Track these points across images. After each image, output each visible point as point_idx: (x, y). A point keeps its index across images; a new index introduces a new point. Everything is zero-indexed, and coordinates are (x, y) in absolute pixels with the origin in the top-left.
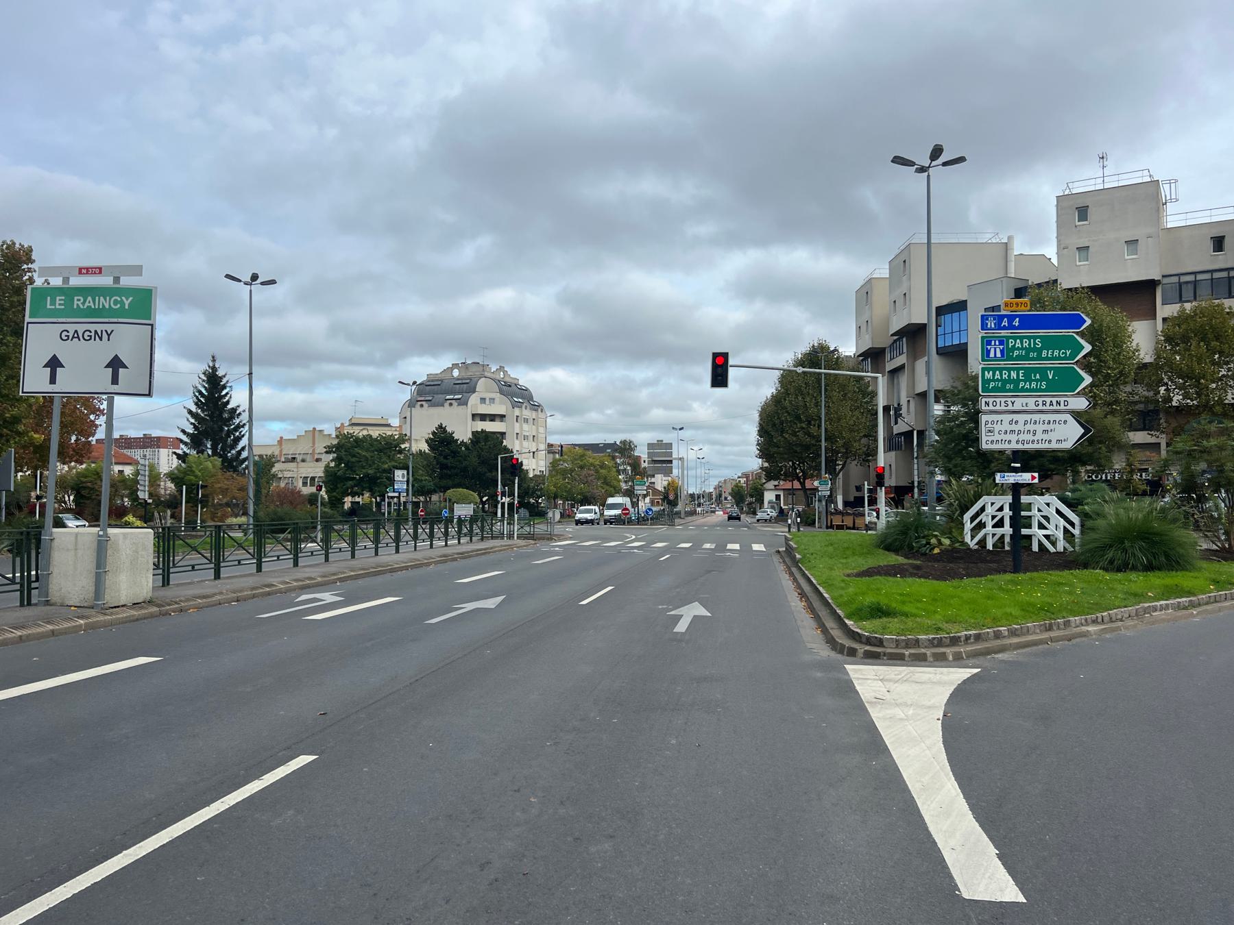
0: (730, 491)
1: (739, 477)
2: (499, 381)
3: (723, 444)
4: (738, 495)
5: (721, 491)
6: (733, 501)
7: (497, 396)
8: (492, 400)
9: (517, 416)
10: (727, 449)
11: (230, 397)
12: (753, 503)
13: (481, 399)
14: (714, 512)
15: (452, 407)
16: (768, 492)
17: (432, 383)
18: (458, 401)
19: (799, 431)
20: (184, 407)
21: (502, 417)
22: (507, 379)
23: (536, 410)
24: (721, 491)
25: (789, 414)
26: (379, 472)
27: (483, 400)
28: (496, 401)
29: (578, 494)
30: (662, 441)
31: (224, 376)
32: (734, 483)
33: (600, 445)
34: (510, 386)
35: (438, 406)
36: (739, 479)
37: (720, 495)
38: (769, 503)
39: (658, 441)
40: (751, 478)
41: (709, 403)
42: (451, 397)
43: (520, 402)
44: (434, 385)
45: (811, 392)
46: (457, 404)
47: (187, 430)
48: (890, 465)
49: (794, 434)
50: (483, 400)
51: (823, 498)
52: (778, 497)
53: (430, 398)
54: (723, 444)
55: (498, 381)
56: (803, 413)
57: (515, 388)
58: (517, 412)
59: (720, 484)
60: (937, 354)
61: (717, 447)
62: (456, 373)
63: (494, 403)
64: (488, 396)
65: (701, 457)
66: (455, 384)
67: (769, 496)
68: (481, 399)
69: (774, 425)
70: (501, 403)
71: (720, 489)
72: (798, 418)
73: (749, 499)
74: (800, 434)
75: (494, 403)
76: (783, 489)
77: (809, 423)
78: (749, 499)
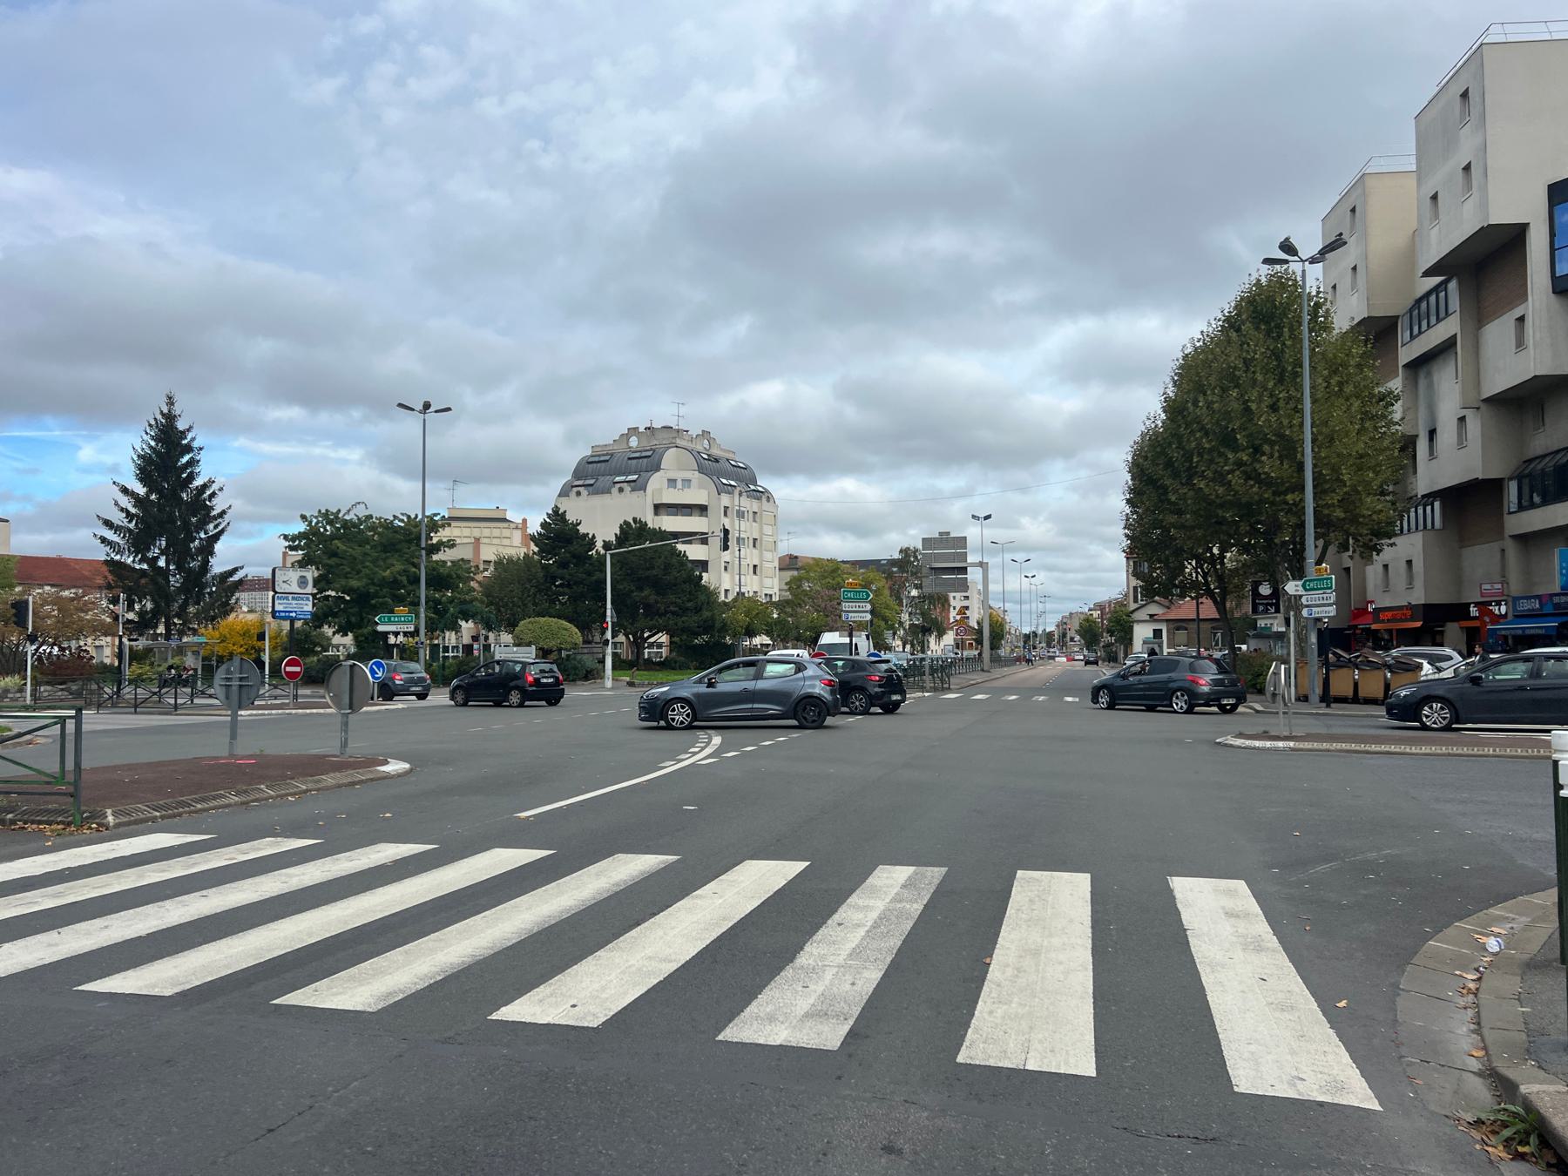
0: (1077, 626)
1: (1090, 610)
2: (699, 453)
3: (1065, 571)
4: (1089, 633)
5: (1065, 629)
6: (1083, 642)
7: (695, 476)
8: (687, 482)
9: (726, 508)
10: (1071, 576)
11: (402, 514)
12: (1112, 644)
13: (669, 480)
14: (1052, 658)
15: (623, 494)
16: (1141, 625)
17: (596, 459)
18: (632, 484)
19: (1231, 472)
20: (114, 483)
21: (702, 509)
22: (715, 452)
23: (759, 499)
24: (1065, 629)
25: (1207, 434)
26: (374, 584)
27: (672, 482)
28: (692, 483)
29: (806, 630)
30: (948, 533)
31: (188, 430)
32: (1082, 617)
33: (883, 562)
34: (717, 461)
35: (602, 493)
36: (1091, 612)
37: (1064, 635)
38: (1144, 643)
39: (941, 534)
40: (1107, 610)
41: (1041, 519)
42: (623, 478)
43: (730, 485)
44: (599, 462)
45: (1259, 377)
46: (630, 489)
47: (116, 522)
48: (1409, 562)
49: (1220, 478)
50: (672, 482)
51: (1311, 623)
52: (1158, 633)
53: (592, 482)
54: (1065, 571)
55: (696, 454)
56: (1243, 428)
57: (727, 464)
58: (725, 500)
59: (1064, 621)
60: (1554, 293)
61: (1056, 574)
62: (634, 442)
63: (689, 487)
64: (680, 475)
65: (1030, 575)
66: (629, 459)
67: (1142, 633)
68: (669, 480)
69: (1169, 464)
70: (701, 486)
71: (1065, 626)
72: (1228, 440)
73: (1107, 638)
74: (1236, 479)
75: (689, 487)
76: (1167, 621)
77: (1257, 450)
78: (1107, 638)
